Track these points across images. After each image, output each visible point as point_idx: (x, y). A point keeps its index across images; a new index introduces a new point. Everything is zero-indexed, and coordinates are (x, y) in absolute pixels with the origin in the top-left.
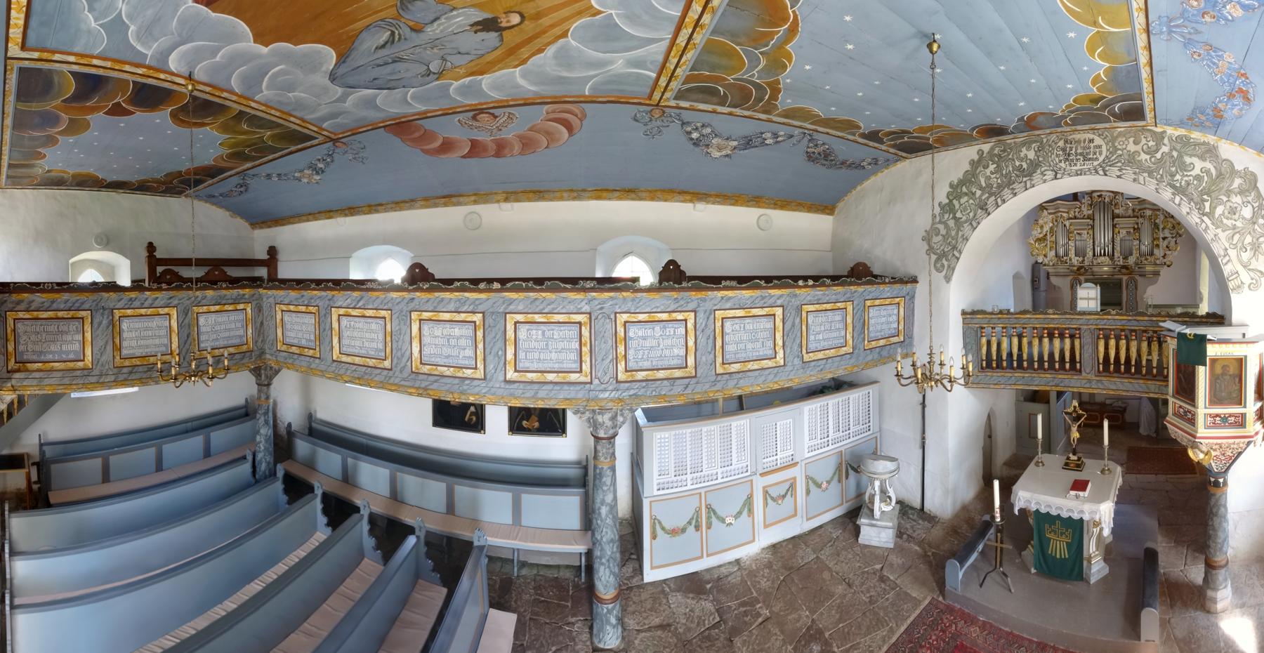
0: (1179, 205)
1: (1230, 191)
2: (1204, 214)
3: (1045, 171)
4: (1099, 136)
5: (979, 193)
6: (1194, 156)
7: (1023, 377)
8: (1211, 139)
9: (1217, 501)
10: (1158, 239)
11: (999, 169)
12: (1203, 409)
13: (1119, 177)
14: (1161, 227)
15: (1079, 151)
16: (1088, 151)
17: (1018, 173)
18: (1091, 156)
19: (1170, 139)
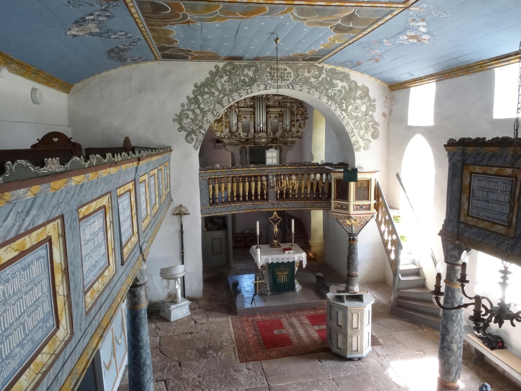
0: (331, 105)
1: (355, 97)
2: (343, 110)
3: (259, 84)
4: (289, 67)
5: (217, 93)
6: (338, 79)
7: (236, 206)
8: (346, 70)
9: (354, 246)
10: (294, 121)
11: (230, 80)
12: (353, 201)
13: (300, 90)
14: (295, 113)
15: (279, 75)
16: (284, 75)
17: (243, 84)
18: (285, 78)
19: (326, 70)
